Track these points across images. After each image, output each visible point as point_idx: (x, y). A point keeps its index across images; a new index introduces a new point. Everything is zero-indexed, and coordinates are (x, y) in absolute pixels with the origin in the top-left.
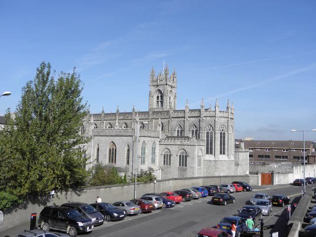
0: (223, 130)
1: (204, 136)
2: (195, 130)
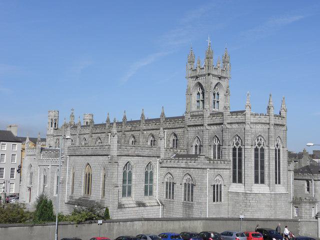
0: (259, 145)
2: (217, 144)
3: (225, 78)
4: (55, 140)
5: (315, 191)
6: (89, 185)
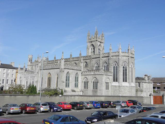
0: (125, 65)
1: (112, 69)
2: (106, 65)
4: (31, 67)
5: (142, 87)
6: (49, 82)
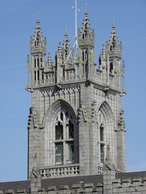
3: (115, 92)
